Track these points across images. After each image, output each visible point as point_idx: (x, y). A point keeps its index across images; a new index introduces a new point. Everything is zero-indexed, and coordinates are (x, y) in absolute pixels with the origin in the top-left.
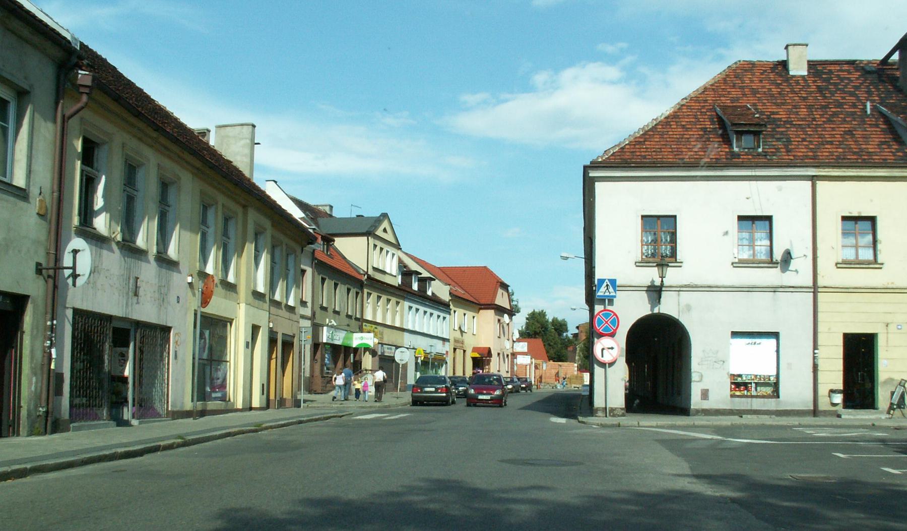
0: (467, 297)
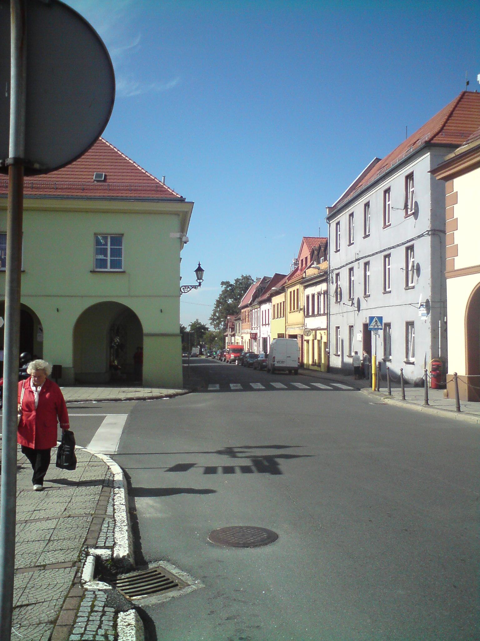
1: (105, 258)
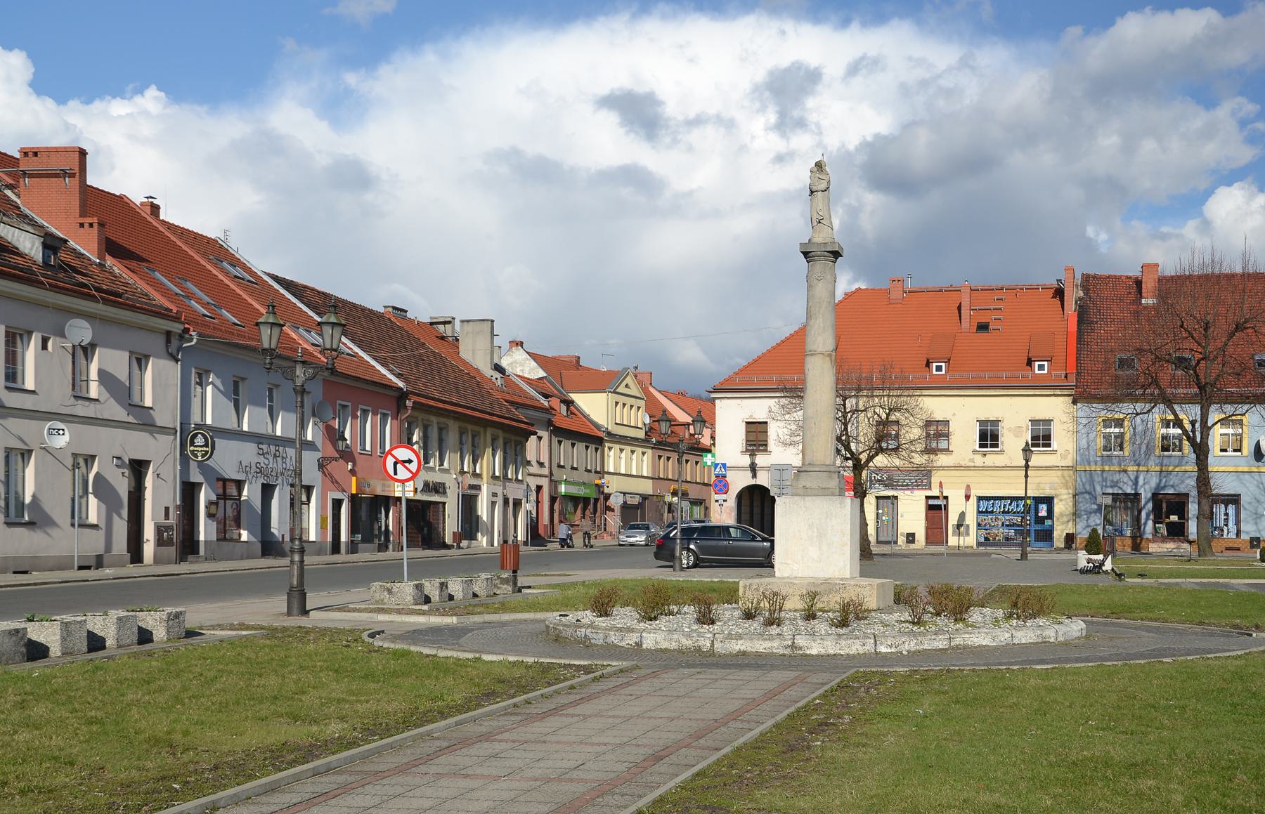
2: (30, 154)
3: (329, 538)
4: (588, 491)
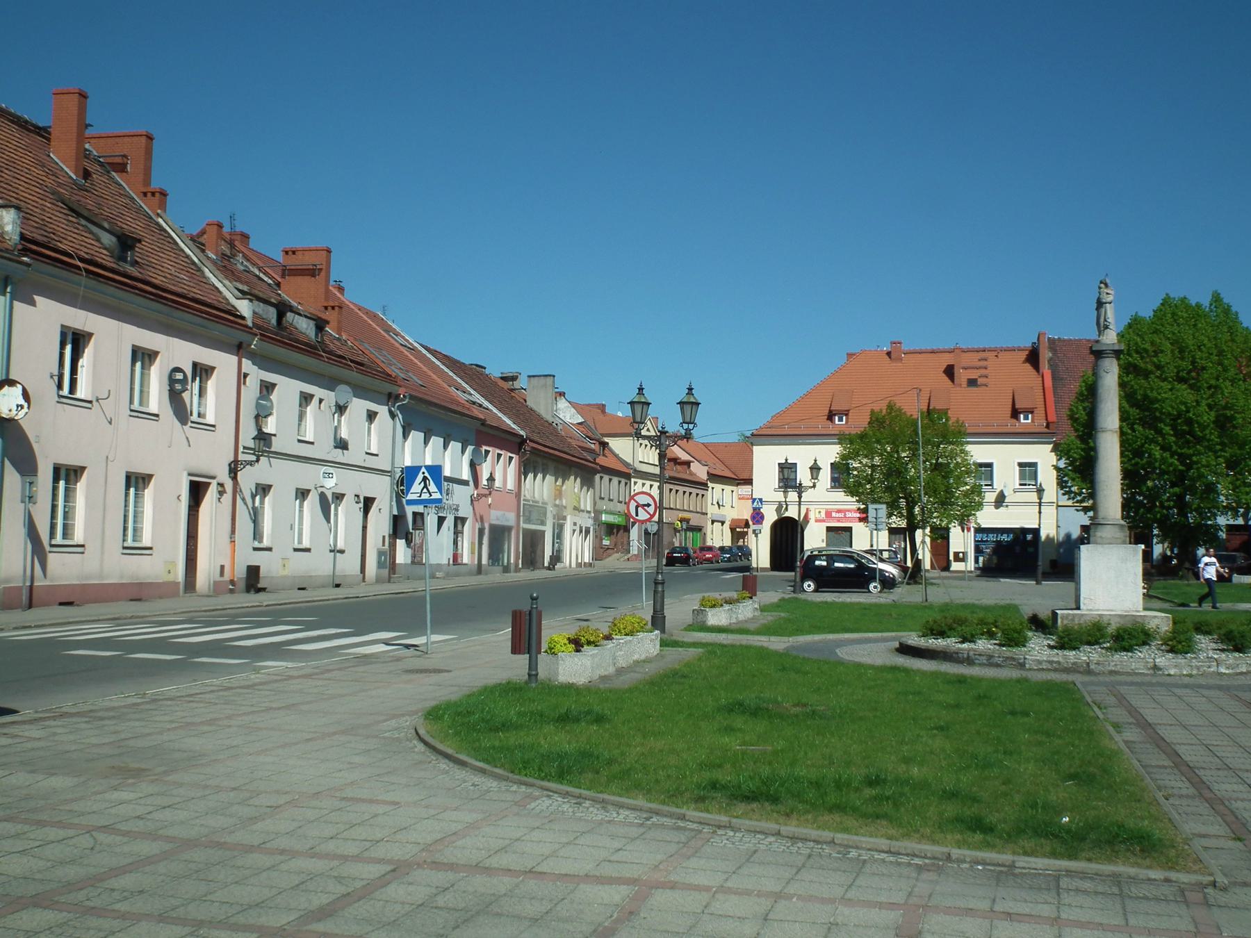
0: (728, 474)
1: (1040, 570)
2: (290, 253)
3: (476, 562)
4: (620, 519)
